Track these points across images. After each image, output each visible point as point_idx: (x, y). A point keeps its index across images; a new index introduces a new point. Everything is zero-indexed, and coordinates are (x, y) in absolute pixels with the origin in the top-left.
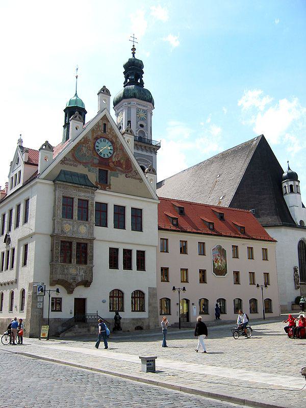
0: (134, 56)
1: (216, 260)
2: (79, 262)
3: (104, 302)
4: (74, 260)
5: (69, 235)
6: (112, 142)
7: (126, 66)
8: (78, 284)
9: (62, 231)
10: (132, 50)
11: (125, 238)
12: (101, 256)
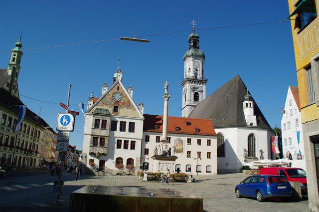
4: (99, 145)
6: (121, 94)
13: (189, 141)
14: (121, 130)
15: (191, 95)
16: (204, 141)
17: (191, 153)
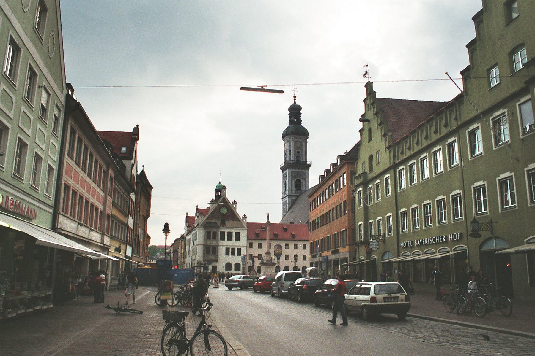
0: (295, 102)
1: (276, 250)
2: (213, 254)
3: (223, 267)
4: (211, 253)
5: (209, 245)
6: (227, 208)
7: (290, 109)
8: (212, 261)
9: (207, 244)
10: (296, 97)
11: (233, 243)
12: (222, 251)
13: (287, 245)
14: (228, 240)
15: (292, 184)
16: (300, 245)
17: (246, 215)
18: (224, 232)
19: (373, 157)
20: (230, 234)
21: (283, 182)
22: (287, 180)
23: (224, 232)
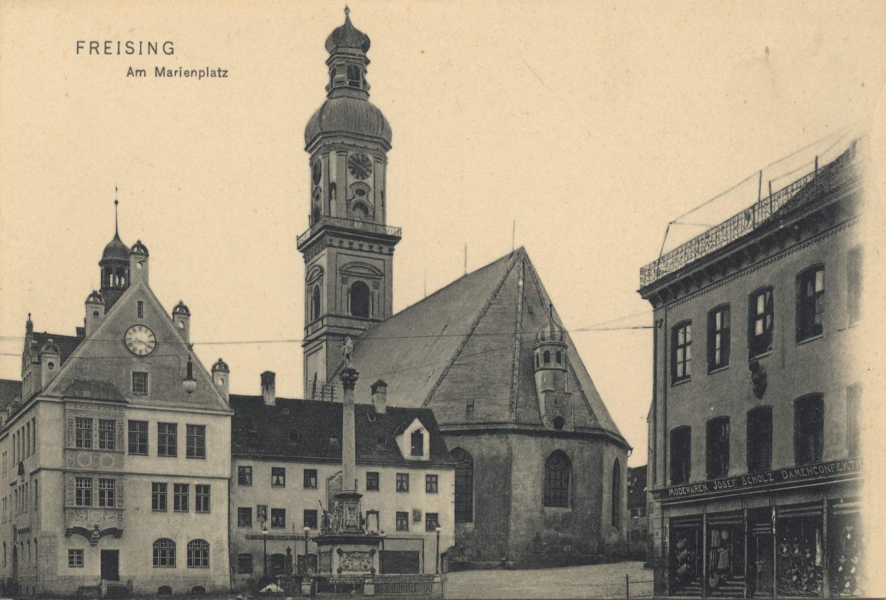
18: (144, 425)
19: (156, 449)
20: (167, 431)
21: (307, 291)
22: (322, 283)
23: (144, 425)
